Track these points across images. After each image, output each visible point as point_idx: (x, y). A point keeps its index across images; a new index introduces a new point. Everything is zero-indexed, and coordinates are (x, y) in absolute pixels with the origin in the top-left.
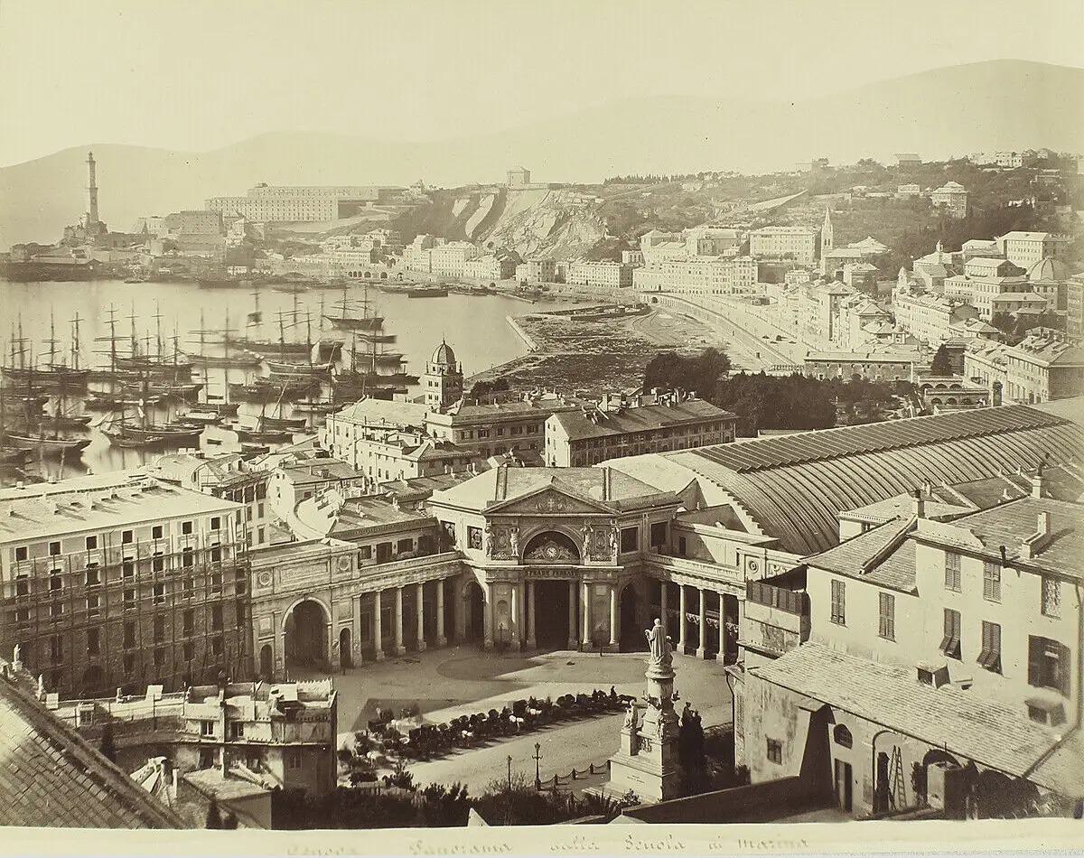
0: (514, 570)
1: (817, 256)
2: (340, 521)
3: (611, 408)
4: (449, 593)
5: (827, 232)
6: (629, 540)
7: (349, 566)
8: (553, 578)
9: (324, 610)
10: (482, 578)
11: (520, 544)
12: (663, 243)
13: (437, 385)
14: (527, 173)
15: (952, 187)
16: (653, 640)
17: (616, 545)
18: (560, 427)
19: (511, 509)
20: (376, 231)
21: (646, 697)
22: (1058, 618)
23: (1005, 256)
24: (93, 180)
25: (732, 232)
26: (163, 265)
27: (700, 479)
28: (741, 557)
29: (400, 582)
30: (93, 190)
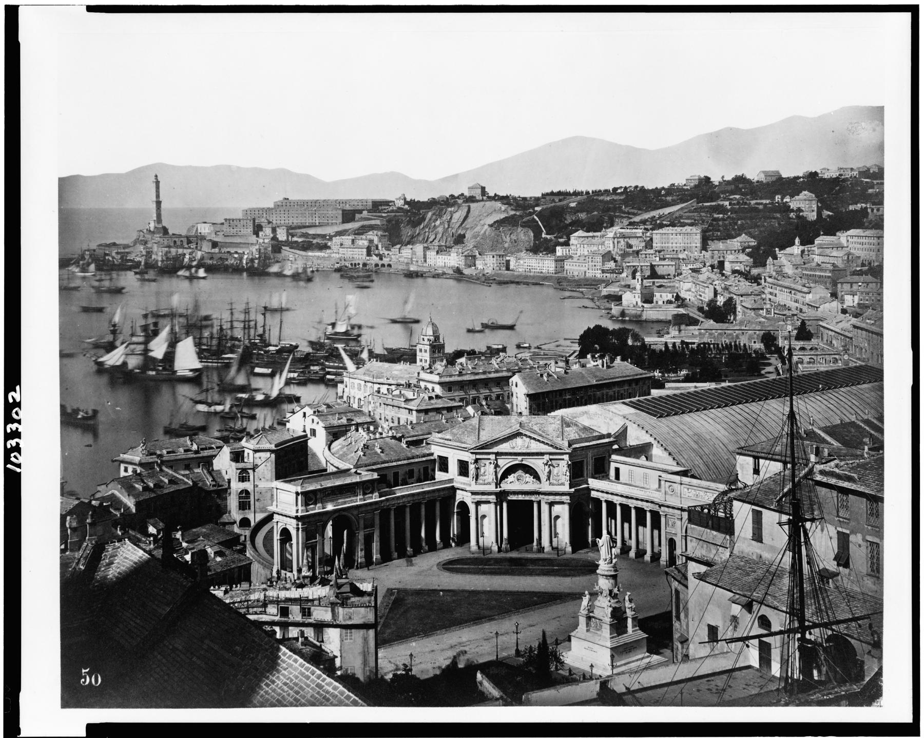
3: (558, 370)
13: (426, 351)
14: (483, 189)
18: (520, 383)
20: (371, 233)
22: (336, 304)
24: (158, 196)
26: (212, 258)
27: (628, 423)
28: (663, 483)
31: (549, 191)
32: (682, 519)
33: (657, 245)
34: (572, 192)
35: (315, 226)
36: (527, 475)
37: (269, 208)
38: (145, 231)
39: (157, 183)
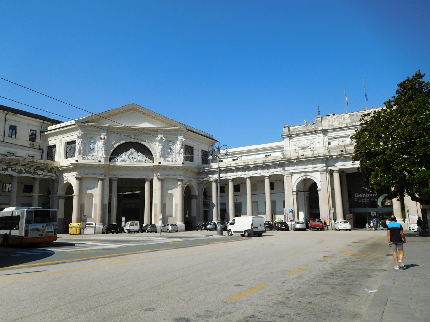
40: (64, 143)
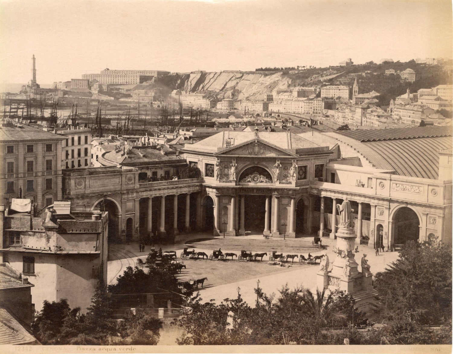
0: (233, 188)
1: (351, 97)
2: (129, 157)
4: (193, 206)
5: (356, 87)
6: (302, 172)
7: (133, 181)
8: (257, 194)
9: (118, 209)
10: (212, 194)
11: (237, 174)
12: (282, 93)
15: (408, 70)
16: (342, 211)
17: (295, 175)
19: (233, 152)
21: (335, 250)
23: (437, 95)
25: (313, 88)
27: (339, 143)
29: (165, 193)
30: (34, 70)
31: (260, 68)
32: (390, 208)
33: (323, 95)
34: (273, 68)
35: (124, 85)
36: (261, 176)
37: (98, 74)
38: (26, 86)
39: (34, 59)
40: (308, 178)
